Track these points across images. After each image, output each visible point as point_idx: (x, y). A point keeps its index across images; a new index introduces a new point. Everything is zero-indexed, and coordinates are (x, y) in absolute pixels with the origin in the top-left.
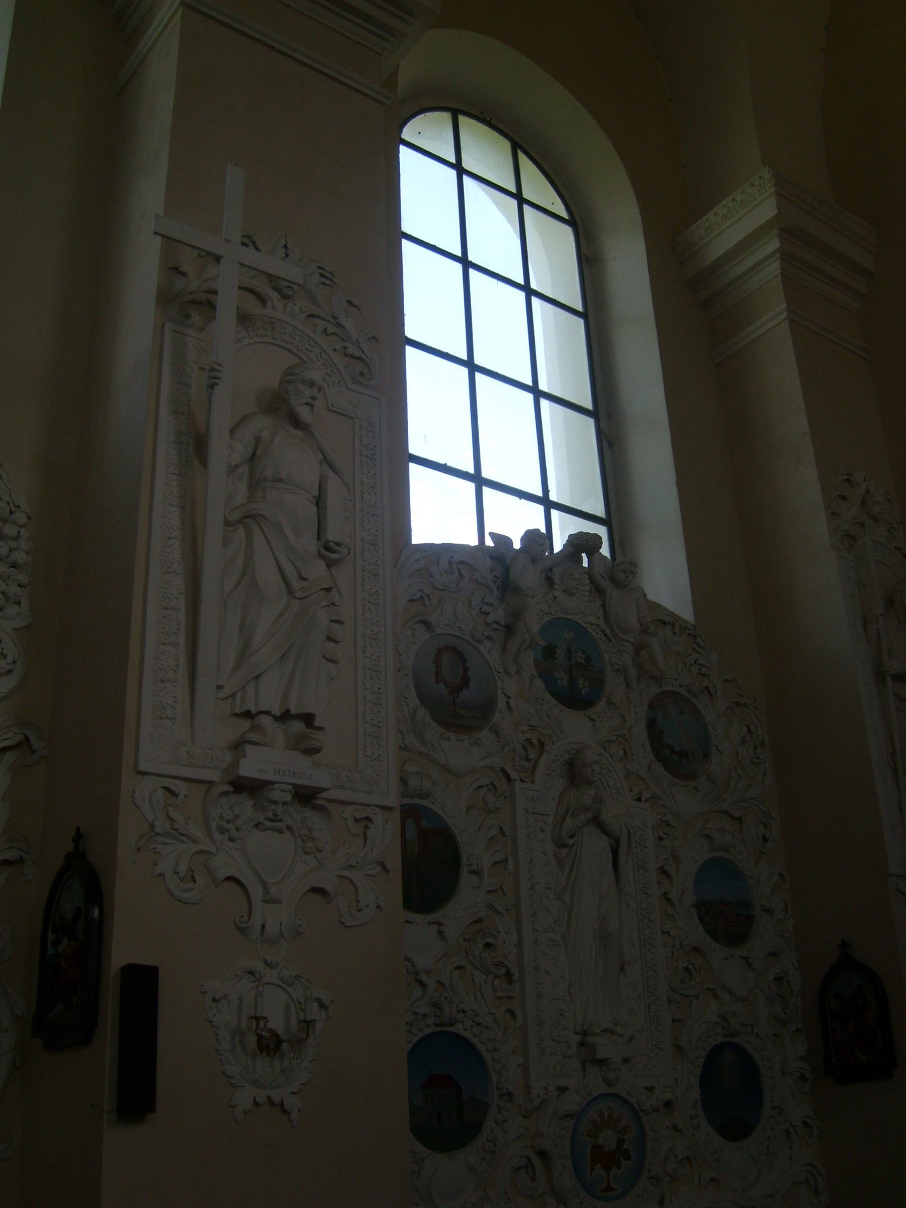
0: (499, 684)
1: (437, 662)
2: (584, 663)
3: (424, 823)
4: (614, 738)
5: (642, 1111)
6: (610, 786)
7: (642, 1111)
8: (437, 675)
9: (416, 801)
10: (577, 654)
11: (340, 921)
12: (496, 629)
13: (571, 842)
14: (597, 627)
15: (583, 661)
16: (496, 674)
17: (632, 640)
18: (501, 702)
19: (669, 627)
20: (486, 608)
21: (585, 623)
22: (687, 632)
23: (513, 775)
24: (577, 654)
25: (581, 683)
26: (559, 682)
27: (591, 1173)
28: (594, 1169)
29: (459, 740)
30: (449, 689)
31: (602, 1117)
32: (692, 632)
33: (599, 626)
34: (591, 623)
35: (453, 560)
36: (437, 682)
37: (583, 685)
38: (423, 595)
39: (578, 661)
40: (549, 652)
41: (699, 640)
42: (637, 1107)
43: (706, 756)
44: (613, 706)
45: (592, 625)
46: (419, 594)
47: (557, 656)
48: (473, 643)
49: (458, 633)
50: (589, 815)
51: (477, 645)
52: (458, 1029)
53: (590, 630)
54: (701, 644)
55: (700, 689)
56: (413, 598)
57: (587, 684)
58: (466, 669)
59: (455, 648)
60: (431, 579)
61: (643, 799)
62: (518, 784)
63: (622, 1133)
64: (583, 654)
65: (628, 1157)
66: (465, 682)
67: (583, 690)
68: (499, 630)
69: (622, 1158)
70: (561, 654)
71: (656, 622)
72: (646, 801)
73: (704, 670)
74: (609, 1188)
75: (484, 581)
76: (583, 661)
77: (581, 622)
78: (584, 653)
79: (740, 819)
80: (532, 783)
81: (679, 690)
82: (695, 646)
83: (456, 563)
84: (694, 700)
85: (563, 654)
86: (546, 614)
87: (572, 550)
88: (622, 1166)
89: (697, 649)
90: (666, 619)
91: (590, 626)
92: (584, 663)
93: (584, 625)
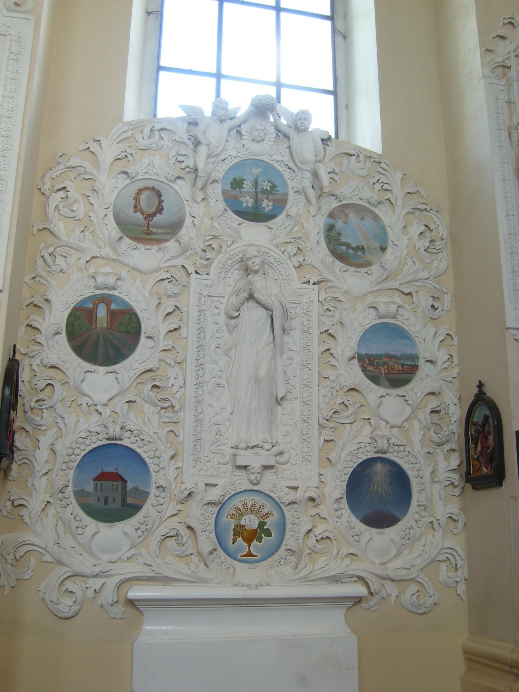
0: (188, 209)
1: (137, 199)
2: (269, 189)
3: (113, 307)
4: (292, 240)
5: (282, 503)
6: (282, 274)
7: (282, 503)
8: (135, 207)
9: (106, 292)
10: (263, 183)
11: (431, 440)
12: (189, 172)
13: (236, 314)
14: (281, 162)
15: (269, 188)
16: (185, 202)
17: (309, 168)
18: (188, 220)
19: (353, 158)
20: (180, 158)
21: (272, 161)
22: (373, 160)
23: (191, 270)
24: (263, 183)
25: (265, 204)
26: (244, 205)
27: (233, 543)
28: (236, 541)
29: (146, 249)
30: (145, 216)
31: (245, 506)
32: (377, 160)
33: (283, 161)
34: (276, 160)
35: (154, 128)
36: (135, 212)
37: (267, 205)
38: (127, 154)
39: (263, 188)
40: (237, 184)
41: (383, 165)
42: (278, 501)
43: (383, 249)
44: (290, 217)
45: (277, 161)
46: (123, 155)
47: (244, 186)
48: (168, 183)
49: (155, 177)
50: (246, 295)
51: (171, 184)
52: (126, 442)
53: (276, 165)
54: (385, 167)
55: (376, 200)
56: (118, 157)
57: (271, 203)
58: (161, 202)
59: (153, 188)
60: (137, 144)
61: (312, 282)
62: (194, 276)
63: (263, 518)
64: (269, 183)
65: (268, 533)
66: (160, 210)
67: (266, 208)
68: (190, 172)
69: (263, 535)
70: (248, 185)
71: (342, 155)
72: (314, 284)
73: (386, 186)
74: (250, 554)
75: (181, 140)
76: (269, 188)
77: (268, 161)
78: (269, 182)
79: (410, 294)
80: (207, 274)
81: (360, 202)
82: (380, 169)
83: (159, 131)
84: (373, 209)
85: (250, 185)
86: (235, 157)
87: (253, 109)
88: (263, 540)
89: (382, 171)
90: (351, 152)
91: (276, 162)
92: (269, 189)
93: (271, 162)
